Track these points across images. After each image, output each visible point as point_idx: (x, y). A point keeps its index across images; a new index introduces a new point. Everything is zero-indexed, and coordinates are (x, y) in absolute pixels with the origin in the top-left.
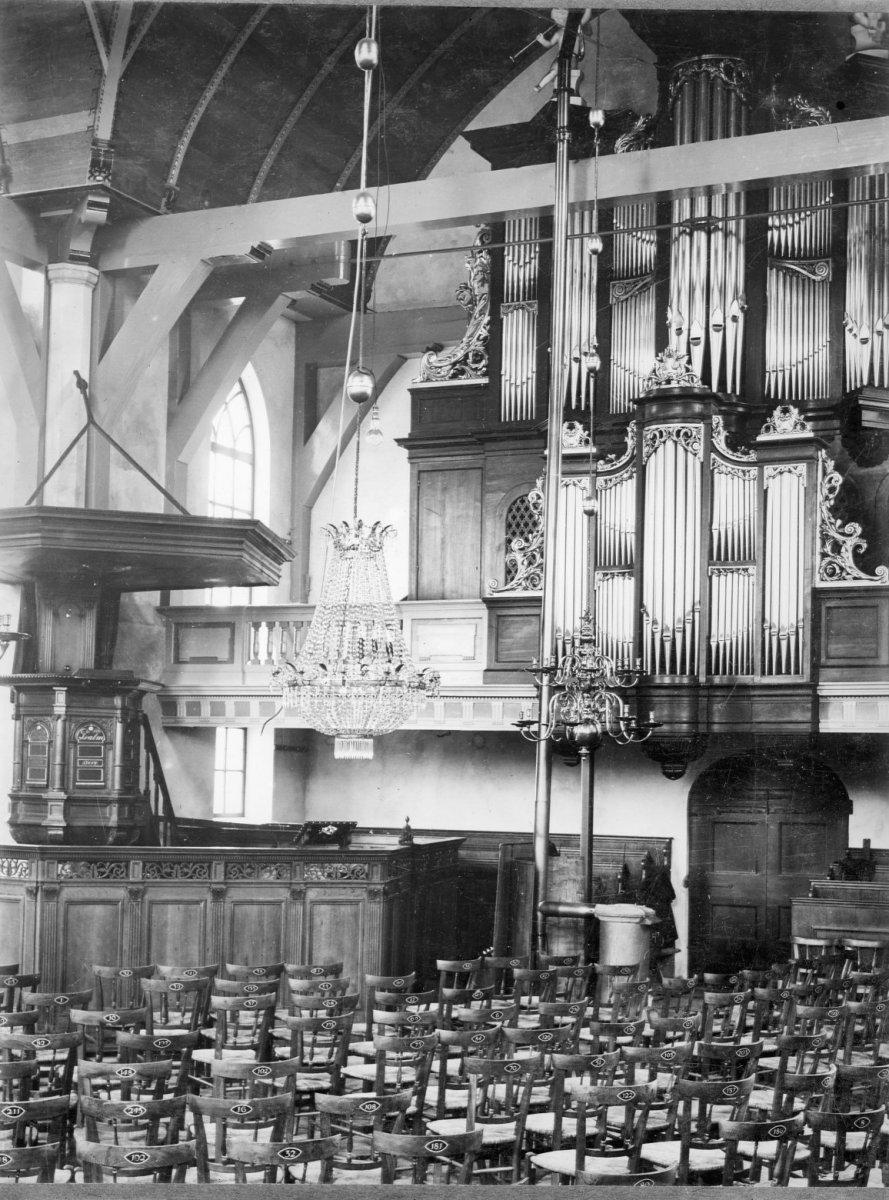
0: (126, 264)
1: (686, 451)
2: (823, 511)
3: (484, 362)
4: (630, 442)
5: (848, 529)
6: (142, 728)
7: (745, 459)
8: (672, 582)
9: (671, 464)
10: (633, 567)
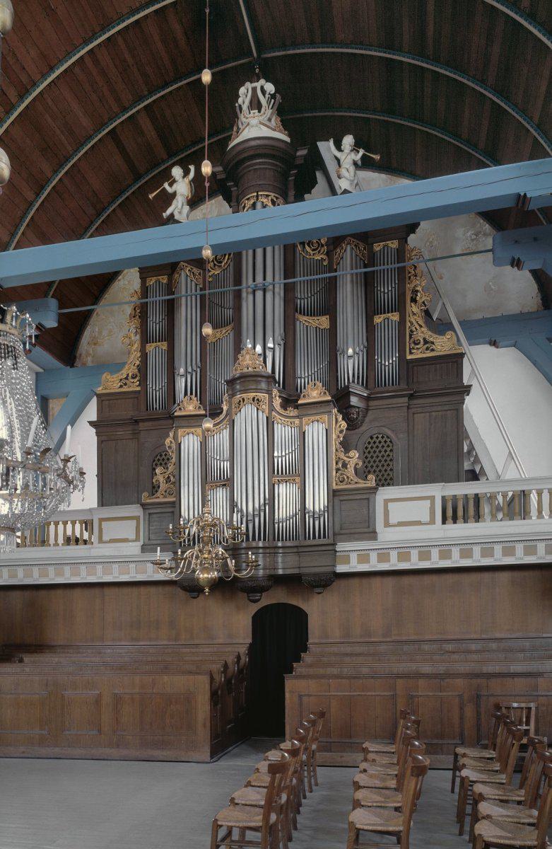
1: (258, 409)
2: (334, 445)
3: (138, 378)
4: (225, 408)
9: (249, 418)
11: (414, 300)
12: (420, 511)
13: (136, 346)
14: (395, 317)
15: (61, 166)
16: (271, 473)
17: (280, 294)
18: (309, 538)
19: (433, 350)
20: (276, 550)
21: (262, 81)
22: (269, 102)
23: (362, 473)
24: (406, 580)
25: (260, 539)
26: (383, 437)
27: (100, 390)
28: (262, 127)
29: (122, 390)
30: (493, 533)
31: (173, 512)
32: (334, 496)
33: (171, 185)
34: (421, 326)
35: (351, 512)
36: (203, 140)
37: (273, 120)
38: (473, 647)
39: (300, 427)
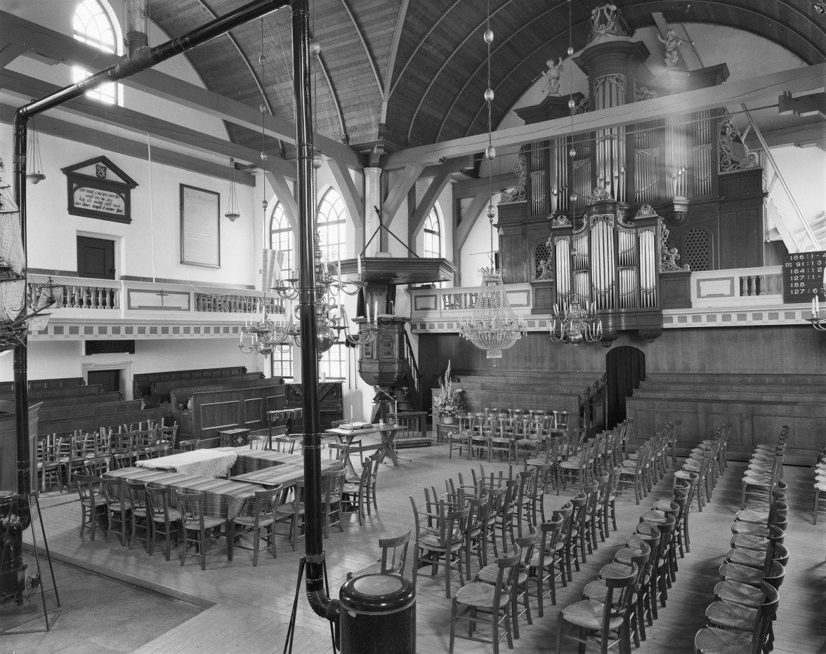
4: (585, 222)
5: (672, 251)
7: (630, 226)
10: (587, 269)
12: (724, 287)
23: (680, 263)
24: (716, 333)
25: (609, 308)
29: (515, 202)
30: (754, 305)
31: (551, 288)
32: (660, 278)
34: (729, 151)
35: (674, 289)
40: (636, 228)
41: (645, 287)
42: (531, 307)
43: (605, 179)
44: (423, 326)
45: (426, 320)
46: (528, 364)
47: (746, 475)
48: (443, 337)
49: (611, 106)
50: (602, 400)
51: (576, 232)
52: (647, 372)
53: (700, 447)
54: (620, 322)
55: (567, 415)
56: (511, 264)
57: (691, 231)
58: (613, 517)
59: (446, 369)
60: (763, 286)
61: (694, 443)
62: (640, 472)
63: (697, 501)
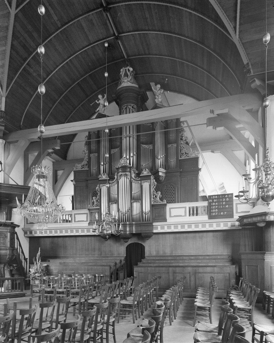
0: (10, 141)
1: (127, 178)
4: (116, 177)
5: (158, 193)
6: (15, 234)
7: (138, 179)
8: (124, 204)
9: (123, 181)
10: (117, 202)
11: (182, 139)
12: (181, 212)
13: (87, 154)
14: (175, 145)
15: (61, 95)
16: (131, 199)
17: (135, 138)
18: (144, 221)
19: (188, 156)
20: (133, 225)
21: (128, 67)
22: (131, 74)
23: (161, 199)
24: (178, 235)
25: (127, 221)
26: (171, 186)
27: (75, 169)
28: (128, 82)
29: (82, 169)
31: (99, 212)
32: (152, 207)
33: (98, 101)
34: (184, 148)
35: (158, 212)
36: (105, 86)
37: (132, 80)
38: (200, 258)
39: (141, 184)
40: (140, 180)
41: (145, 211)
42: (88, 222)
43: (126, 157)
44: (31, 233)
45: (32, 229)
46: (87, 253)
47: (196, 302)
48: (42, 239)
49: (130, 113)
50: (123, 270)
51: (111, 182)
52: (145, 255)
53: (170, 289)
54: (133, 229)
55: (104, 276)
56: (80, 201)
57: (167, 186)
58: (114, 333)
59: (38, 252)
60: (199, 211)
61: (168, 288)
62: (136, 303)
63: (168, 319)
